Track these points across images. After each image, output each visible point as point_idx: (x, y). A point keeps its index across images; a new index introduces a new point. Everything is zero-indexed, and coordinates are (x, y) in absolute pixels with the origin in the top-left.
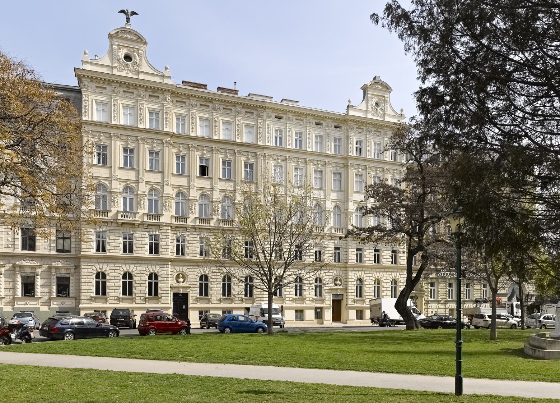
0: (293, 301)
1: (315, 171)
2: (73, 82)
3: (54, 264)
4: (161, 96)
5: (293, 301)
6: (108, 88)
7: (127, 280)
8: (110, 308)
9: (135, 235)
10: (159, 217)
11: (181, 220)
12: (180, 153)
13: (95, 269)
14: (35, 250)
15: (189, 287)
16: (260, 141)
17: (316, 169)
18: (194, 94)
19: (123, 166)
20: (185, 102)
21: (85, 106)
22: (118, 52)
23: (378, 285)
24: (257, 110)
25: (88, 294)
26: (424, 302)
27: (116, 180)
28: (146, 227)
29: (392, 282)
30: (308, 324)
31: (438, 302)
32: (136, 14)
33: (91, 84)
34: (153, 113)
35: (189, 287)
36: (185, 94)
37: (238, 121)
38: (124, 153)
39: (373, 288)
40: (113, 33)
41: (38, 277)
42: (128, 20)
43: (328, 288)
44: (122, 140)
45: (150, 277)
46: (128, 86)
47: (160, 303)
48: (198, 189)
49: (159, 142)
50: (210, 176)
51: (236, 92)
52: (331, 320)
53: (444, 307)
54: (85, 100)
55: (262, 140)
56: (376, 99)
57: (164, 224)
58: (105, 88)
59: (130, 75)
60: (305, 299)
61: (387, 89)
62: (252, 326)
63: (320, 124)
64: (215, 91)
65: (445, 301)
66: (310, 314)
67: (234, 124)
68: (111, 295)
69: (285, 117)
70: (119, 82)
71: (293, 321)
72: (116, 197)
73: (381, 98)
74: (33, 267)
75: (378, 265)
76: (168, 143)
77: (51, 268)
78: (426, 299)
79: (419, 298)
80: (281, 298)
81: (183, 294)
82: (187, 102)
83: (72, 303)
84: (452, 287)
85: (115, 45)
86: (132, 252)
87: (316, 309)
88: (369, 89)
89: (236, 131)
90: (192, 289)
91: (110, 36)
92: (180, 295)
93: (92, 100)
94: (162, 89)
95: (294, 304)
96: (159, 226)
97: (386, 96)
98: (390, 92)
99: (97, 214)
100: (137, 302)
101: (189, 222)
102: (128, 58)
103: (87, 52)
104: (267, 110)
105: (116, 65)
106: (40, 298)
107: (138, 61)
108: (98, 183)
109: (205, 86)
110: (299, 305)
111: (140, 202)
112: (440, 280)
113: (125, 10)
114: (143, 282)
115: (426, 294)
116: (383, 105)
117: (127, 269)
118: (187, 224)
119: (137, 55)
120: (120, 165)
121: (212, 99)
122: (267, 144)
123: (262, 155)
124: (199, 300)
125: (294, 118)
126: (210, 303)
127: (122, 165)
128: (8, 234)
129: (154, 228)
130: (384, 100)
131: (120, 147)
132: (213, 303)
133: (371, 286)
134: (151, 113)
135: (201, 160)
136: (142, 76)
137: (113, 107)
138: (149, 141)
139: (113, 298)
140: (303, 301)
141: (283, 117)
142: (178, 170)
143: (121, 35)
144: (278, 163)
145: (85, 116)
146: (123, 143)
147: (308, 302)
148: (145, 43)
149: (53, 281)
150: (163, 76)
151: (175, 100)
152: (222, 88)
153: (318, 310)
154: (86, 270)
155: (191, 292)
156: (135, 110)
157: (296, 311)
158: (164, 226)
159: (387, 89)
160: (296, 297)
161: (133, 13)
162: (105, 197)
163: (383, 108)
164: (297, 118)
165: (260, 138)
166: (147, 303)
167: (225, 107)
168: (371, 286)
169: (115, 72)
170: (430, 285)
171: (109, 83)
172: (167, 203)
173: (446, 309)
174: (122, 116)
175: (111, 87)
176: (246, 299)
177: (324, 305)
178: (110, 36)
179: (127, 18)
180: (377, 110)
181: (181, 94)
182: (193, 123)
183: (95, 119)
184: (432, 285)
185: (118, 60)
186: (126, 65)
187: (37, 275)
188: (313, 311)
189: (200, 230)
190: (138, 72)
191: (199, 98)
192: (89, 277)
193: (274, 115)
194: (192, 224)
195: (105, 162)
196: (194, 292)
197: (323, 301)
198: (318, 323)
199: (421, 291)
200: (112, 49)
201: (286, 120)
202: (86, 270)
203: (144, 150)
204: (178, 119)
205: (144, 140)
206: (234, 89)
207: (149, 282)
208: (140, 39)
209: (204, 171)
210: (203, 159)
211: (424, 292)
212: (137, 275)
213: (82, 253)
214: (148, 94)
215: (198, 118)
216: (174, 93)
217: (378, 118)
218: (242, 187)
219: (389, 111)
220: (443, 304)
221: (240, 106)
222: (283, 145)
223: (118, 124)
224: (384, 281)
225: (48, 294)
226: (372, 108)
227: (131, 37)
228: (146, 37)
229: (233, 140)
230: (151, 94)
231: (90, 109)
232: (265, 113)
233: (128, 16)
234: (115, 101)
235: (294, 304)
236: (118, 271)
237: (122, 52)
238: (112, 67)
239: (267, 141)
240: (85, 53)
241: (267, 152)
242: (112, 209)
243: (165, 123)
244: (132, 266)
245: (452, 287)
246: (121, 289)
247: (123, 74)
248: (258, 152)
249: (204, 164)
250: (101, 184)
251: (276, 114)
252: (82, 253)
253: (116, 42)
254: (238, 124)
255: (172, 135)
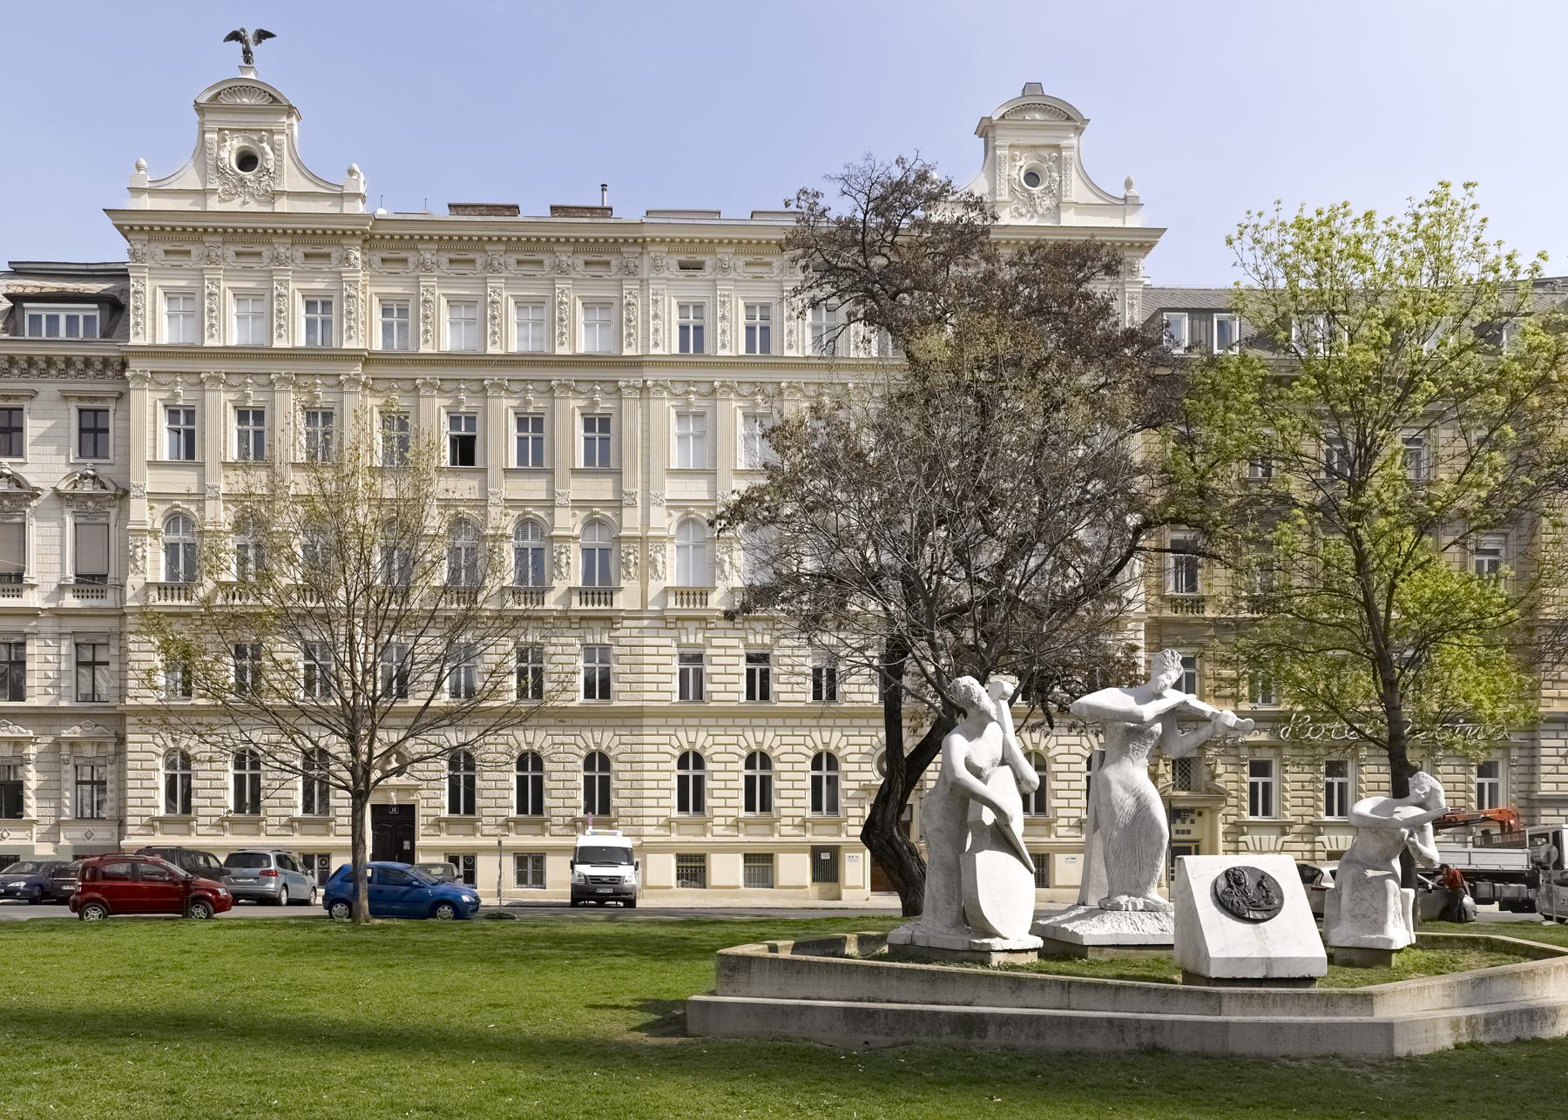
0: (1081, 827)
1: (680, 416)
2: (114, 250)
3: (65, 733)
4: (335, 252)
5: (804, 826)
6: (195, 250)
7: (824, 773)
8: (222, 848)
9: (550, 650)
10: (608, 594)
11: (596, 597)
12: (245, 401)
13: (582, 745)
14: (23, 700)
15: (416, 789)
16: (494, 343)
17: (684, 409)
18: (495, 233)
19: (515, 466)
20: (405, 261)
21: (137, 308)
22: (219, 148)
23: (831, 773)
24: (621, 253)
25: (144, 811)
26: (1221, 828)
27: (216, 498)
28: (672, 626)
29: (1089, 761)
30: (786, 897)
31: (1283, 828)
32: (270, 35)
33: (153, 245)
34: (316, 303)
35: (416, 789)
36: (402, 237)
37: (562, 292)
38: (239, 423)
39: (1084, 781)
40: (203, 100)
41: (30, 767)
42: (247, 55)
43: (856, 785)
44: (229, 387)
45: (683, 762)
46: (245, 238)
47: (263, 835)
48: (579, 504)
49: (332, 381)
50: (479, 464)
51: (606, 211)
52: (868, 887)
53: (1308, 847)
54: (136, 292)
55: (144, 329)
56: (1025, 162)
57: (623, 614)
58: (188, 253)
59: (253, 207)
60: (778, 820)
61: (1069, 118)
62: (420, 900)
63: (699, 266)
64: (443, 213)
65: (1311, 824)
66: (795, 869)
67: (267, 298)
68: (201, 811)
69: (709, 261)
70: (572, 240)
71: (738, 887)
72: (139, 544)
73: (1045, 153)
74: (18, 743)
75: (603, 703)
76: (355, 381)
77: (59, 744)
78: (1231, 819)
79: (1206, 813)
80: (833, 818)
81: (400, 807)
82: (412, 257)
83: (113, 834)
84: (1497, 776)
85: (212, 131)
86: (608, 697)
87: (816, 851)
88: (999, 132)
89: (555, 324)
90: (425, 793)
91: (200, 108)
92: (394, 810)
93: (155, 290)
94: (334, 233)
95: (741, 835)
96: (609, 621)
97: (1064, 143)
98: (1079, 130)
99: (166, 595)
100: (270, 830)
101: (551, 602)
102: (247, 161)
103: (143, 162)
104: (650, 248)
105: (215, 184)
106: (34, 821)
107: (271, 165)
108: (170, 512)
109: (513, 209)
110: (757, 840)
111: (559, 560)
112: (1287, 753)
113: (238, 29)
114: (569, 776)
115: (1231, 801)
116: (1055, 175)
117: (527, 743)
118: (546, 607)
119: (268, 149)
120: (507, 463)
121: (480, 239)
122: (653, 351)
123: (634, 387)
124: (674, 825)
125: (740, 261)
126: (478, 835)
127: (580, 463)
128: (47, 662)
129: (596, 625)
130: (1058, 160)
131: (225, 408)
132: (485, 832)
133: (1077, 776)
134: (310, 306)
135: (454, 421)
136: (283, 205)
137: (206, 302)
138: (582, 388)
139: (721, 821)
140: (771, 825)
141: (703, 263)
142: (589, 458)
143: (226, 100)
144: (689, 404)
145: (137, 334)
146: (515, 403)
147: (785, 830)
148: (290, 111)
149: (64, 776)
150: (342, 196)
151: (377, 257)
152: (563, 208)
153: (825, 856)
154: (138, 747)
155: (423, 803)
156: (261, 302)
157: (748, 858)
158: (624, 618)
159: (1069, 118)
160: (817, 815)
161: (263, 35)
162: (538, 552)
163: (1055, 187)
164: (749, 259)
165: (630, 335)
166: (296, 835)
167: (521, 257)
168: (1077, 776)
169: (214, 204)
170: (1247, 769)
171: (195, 237)
172: (631, 557)
173: (1313, 851)
174: (514, 331)
175: (201, 247)
176: (680, 823)
177: (844, 838)
178: (986, 130)
179: (244, 52)
180: (1030, 195)
181: (392, 237)
182: (426, 317)
183: (164, 338)
184: (1260, 768)
185: (221, 171)
186: (241, 180)
187: (28, 762)
188: (807, 859)
189: (584, 624)
190: (274, 195)
191: (511, 244)
192: (146, 765)
193: (673, 261)
194: (560, 607)
195: (190, 454)
196: (433, 801)
197: (839, 826)
198: (823, 897)
199: (1209, 791)
200: (203, 146)
201: (715, 269)
202: (138, 747)
203: (288, 413)
204: (386, 312)
205: (567, 387)
206: (600, 205)
207: (813, 778)
208: (276, 104)
209: (465, 451)
210: (178, 412)
211: (1221, 795)
212: (621, 758)
213: (129, 701)
214: (299, 252)
215: (443, 301)
216: (372, 237)
217: (1034, 222)
218: (224, 483)
219: (1075, 190)
220: (1301, 834)
221: (565, 249)
222: (708, 350)
223: (221, 344)
224: (1059, 759)
225: (53, 812)
226: (1012, 190)
227: (253, 101)
228: (289, 94)
229: (547, 351)
230: (309, 250)
231: (148, 315)
232: (645, 257)
233: (247, 45)
234: (212, 284)
235: (741, 835)
236: (668, 748)
237: (229, 148)
238: (204, 193)
239: (651, 343)
240: (139, 167)
241: (650, 375)
242: (555, 583)
243: (345, 326)
244: (608, 734)
245: (1497, 776)
246: (513, 797)
247: (235, 205)
248: (624, 378)
249: (463, 432)
250: (178, 513)
251: (683, 258)
252: (129, 701)
253: (215, 121)
254: (561, 303)
255: (368, 359)
